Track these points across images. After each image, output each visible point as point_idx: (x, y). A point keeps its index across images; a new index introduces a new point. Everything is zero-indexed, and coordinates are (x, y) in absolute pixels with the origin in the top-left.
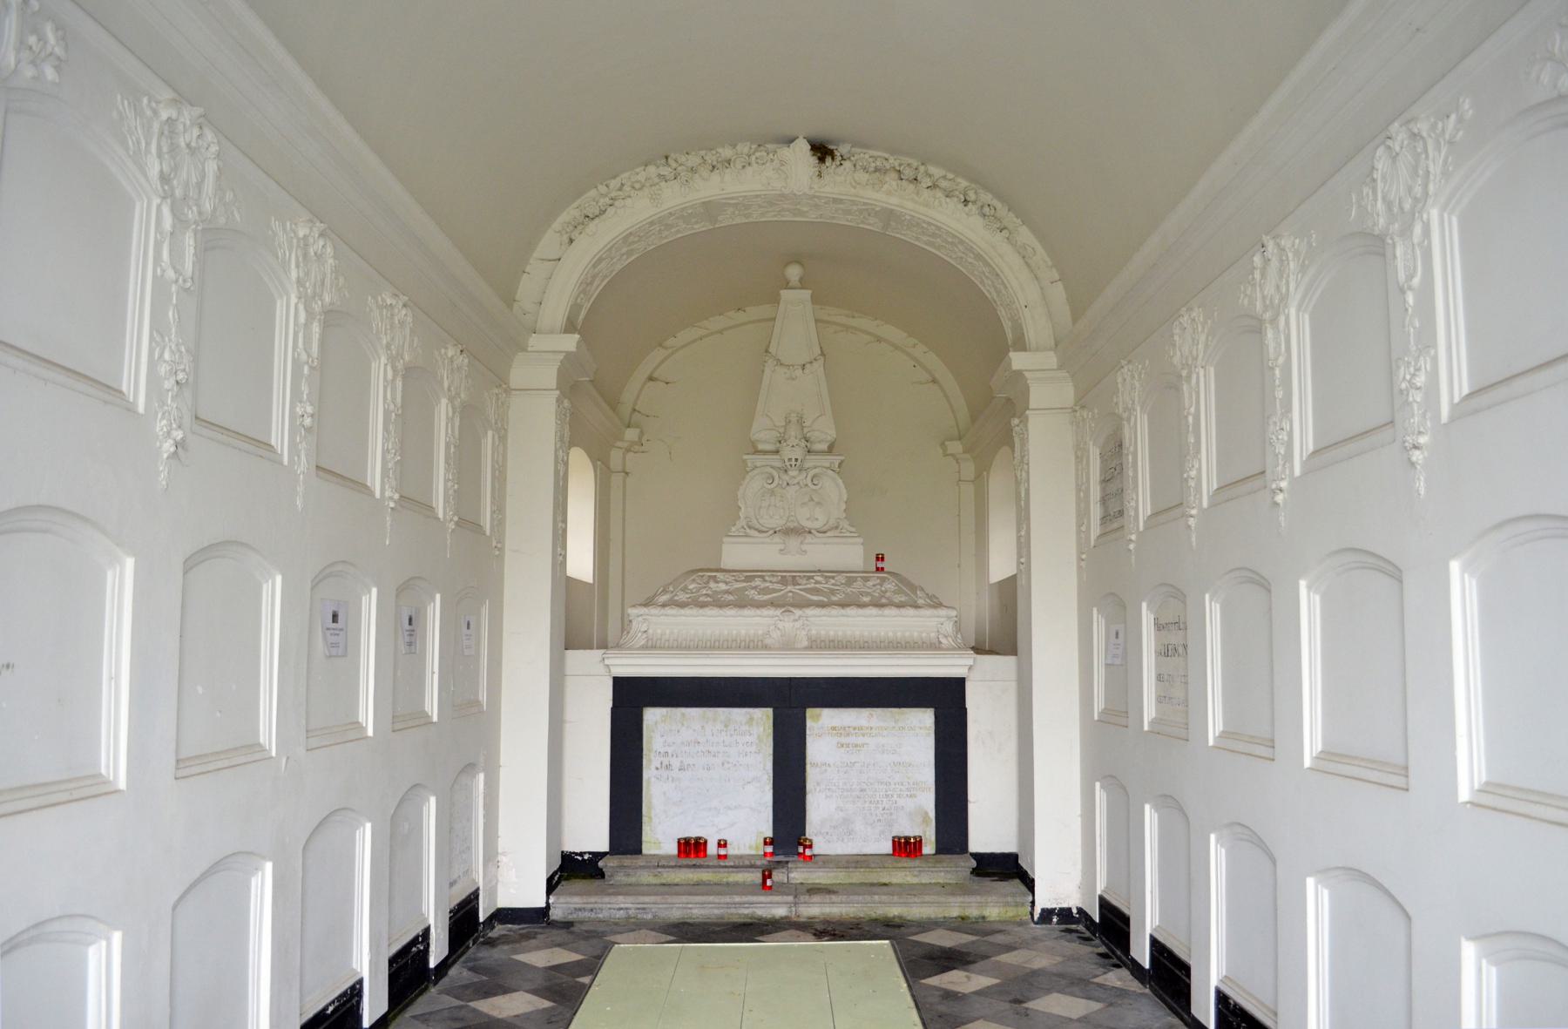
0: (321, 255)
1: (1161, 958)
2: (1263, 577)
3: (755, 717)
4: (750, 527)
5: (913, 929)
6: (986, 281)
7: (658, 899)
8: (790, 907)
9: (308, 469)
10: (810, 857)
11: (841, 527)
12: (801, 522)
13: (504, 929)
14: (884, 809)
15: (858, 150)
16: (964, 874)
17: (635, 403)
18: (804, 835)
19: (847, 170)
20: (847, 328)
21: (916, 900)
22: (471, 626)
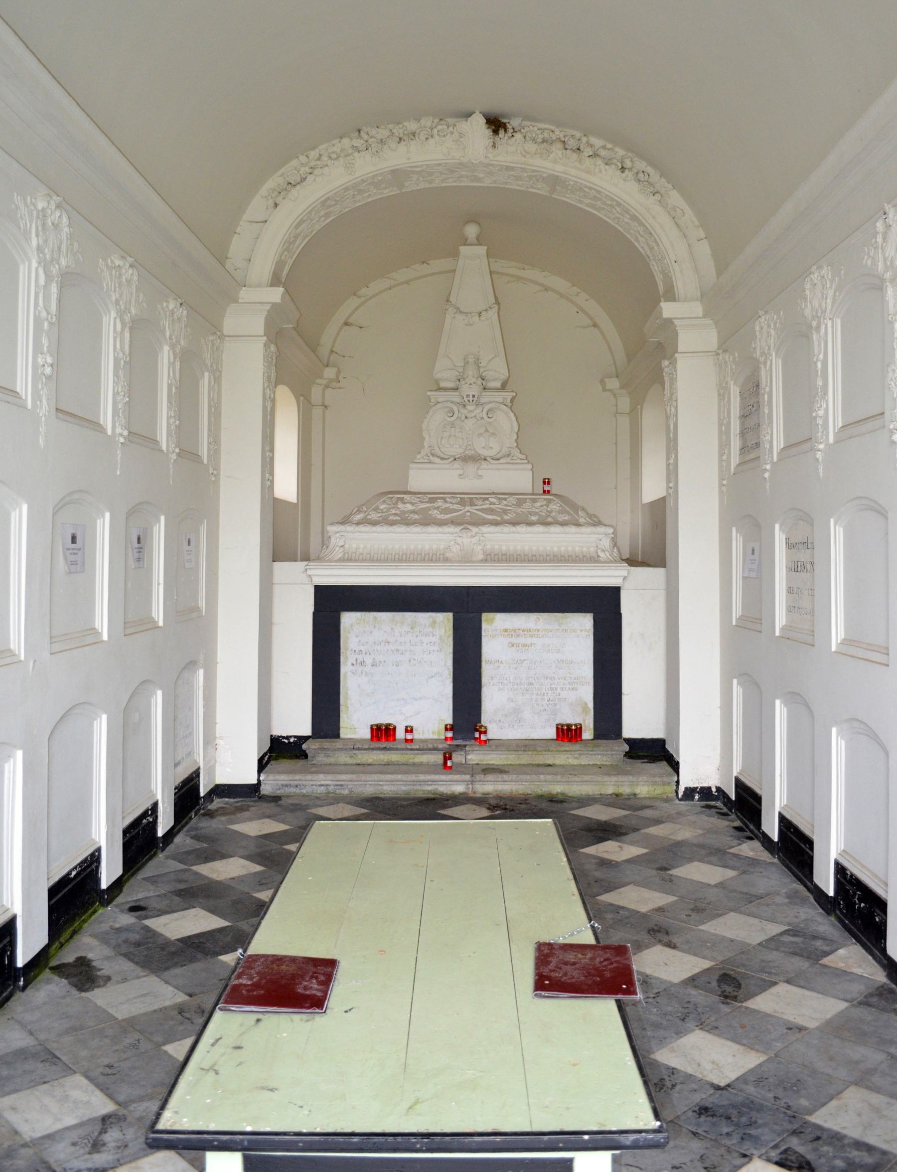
0: (57, 225)
1: (788, 833)
2: (880, 506)
3: (438, 621)
4: (433, 455)
5: (574, 804)
6: (640, 239)
7: (354, 777)
8: (468, 784)
9: (49, 412)
10: (485, 742)
11: (512, 455)
12: (478, 452)
13: (220, 803)
14: (548, 701)
15: (528, 123)
16: (618, 757)
17: (333, 346)
18: (480, 722)
19: (518, 142)
20: (519, 279)
21: (576, 779)
22: (191, 543)
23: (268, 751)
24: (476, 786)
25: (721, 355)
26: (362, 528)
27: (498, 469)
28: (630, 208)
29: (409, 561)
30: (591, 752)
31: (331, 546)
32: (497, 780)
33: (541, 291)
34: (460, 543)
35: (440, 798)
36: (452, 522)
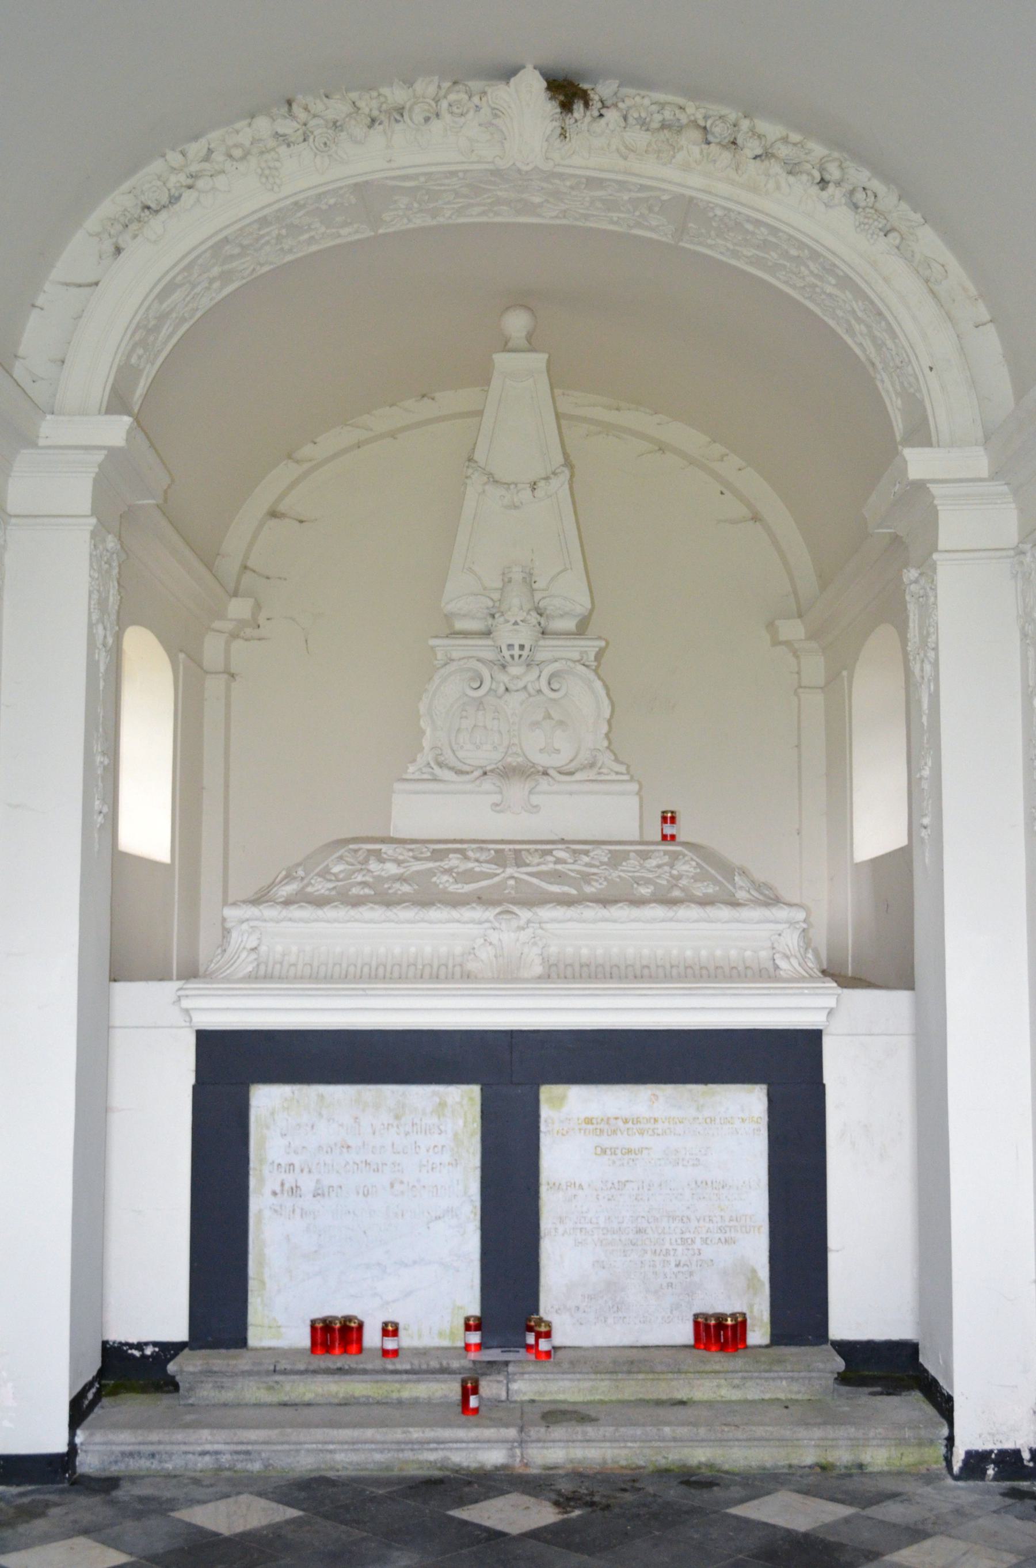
3: (450, 1101)
4: (440, 765)
5: (736, 1491)
7: (273, 1434)
8: (512, 1448)
10: (548, 1354)
11: (599, 765)
12: (532, 760)
14: (677, 1265)
17: (246, 557)
19: (611, 127)
21: (739, 1434)
23: (95, 1379)
24: (530, 1451)
25: (1029, 554)
26: (295, 912)
27: (571, 794)
28: (837, 262)
29: (392, 980)
30: (767, 1375)
31: (231, 950)
32: (575, 1437)
33: (650, 452)
34: (495, 941)
35: (455, 1478)
36: (479, 898)
